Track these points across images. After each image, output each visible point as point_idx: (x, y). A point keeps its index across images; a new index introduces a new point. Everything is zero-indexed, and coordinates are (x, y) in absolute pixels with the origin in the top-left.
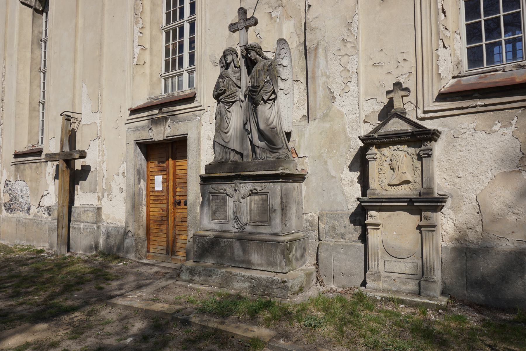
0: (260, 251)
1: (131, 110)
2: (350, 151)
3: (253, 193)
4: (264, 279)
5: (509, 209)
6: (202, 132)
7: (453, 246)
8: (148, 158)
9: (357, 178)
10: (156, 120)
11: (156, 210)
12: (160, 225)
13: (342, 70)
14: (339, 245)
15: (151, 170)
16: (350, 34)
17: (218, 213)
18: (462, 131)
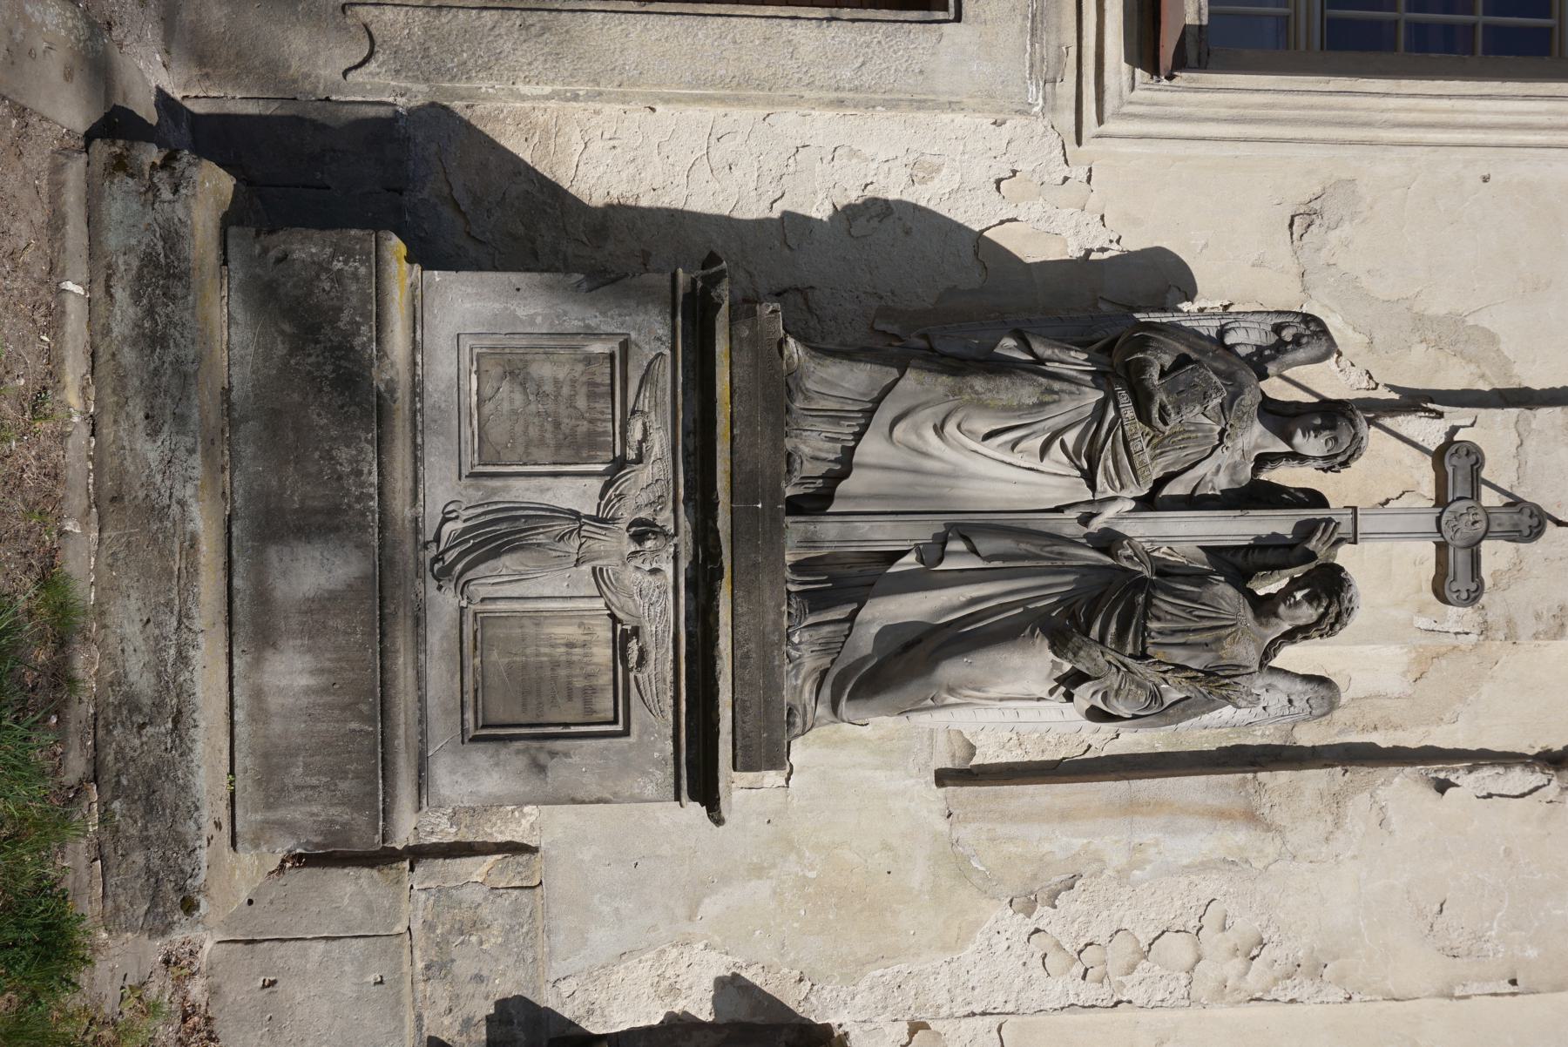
0: (332, 707)
2: (801, 980)
3: (624, 637)
4: (185, 788)
6: (959, 118)
9: (687, 1009)
13: (1138, 942)
14: (399, 965)
16: (1276, 974)
17: (518, 398)
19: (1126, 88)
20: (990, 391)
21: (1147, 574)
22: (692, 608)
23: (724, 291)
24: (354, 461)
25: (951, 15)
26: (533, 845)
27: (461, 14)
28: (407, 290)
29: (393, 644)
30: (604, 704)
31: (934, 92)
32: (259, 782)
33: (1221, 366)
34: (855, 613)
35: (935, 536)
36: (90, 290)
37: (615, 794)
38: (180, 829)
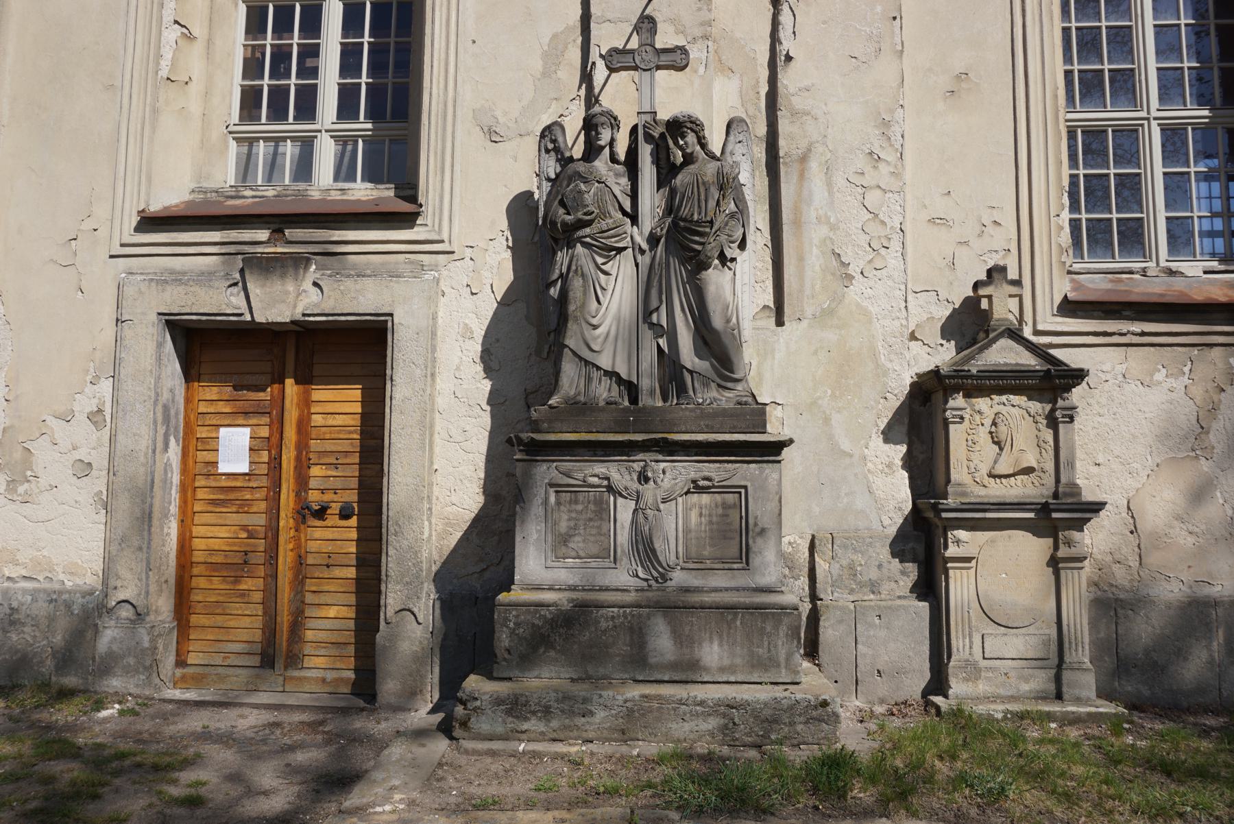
0: (729, 633)
1: (143, 215)
2: (886, 398)
3: (697, 488)
4: (766, 704)
5: (1182, 525)
6: (440, 314)
7: (1092, 596)
8: (190, 372)
10: (264, 262)
11: (223, 532)
12: (237, 579)
14: (870, 607)
15: (202, 409)
17: (577, 539)
18: (1104, 377)
19: (427, 228)
20: (575, 302)
21: (670, 220)
22: (682, 453)
23: (525, 436)
24: (607, 619)
25: (389, 318)
26: (810, 538)
27: (390, 565)
28: (524, 592)
29: (698, 602)
30: (731, 498)
31: (428, 327)
32: (766, 670)
33: (565, 183)
34: (688, 370)
35: (650, 329)
36: (523, 741)
37: (777, 493)
38: (786, 707)
